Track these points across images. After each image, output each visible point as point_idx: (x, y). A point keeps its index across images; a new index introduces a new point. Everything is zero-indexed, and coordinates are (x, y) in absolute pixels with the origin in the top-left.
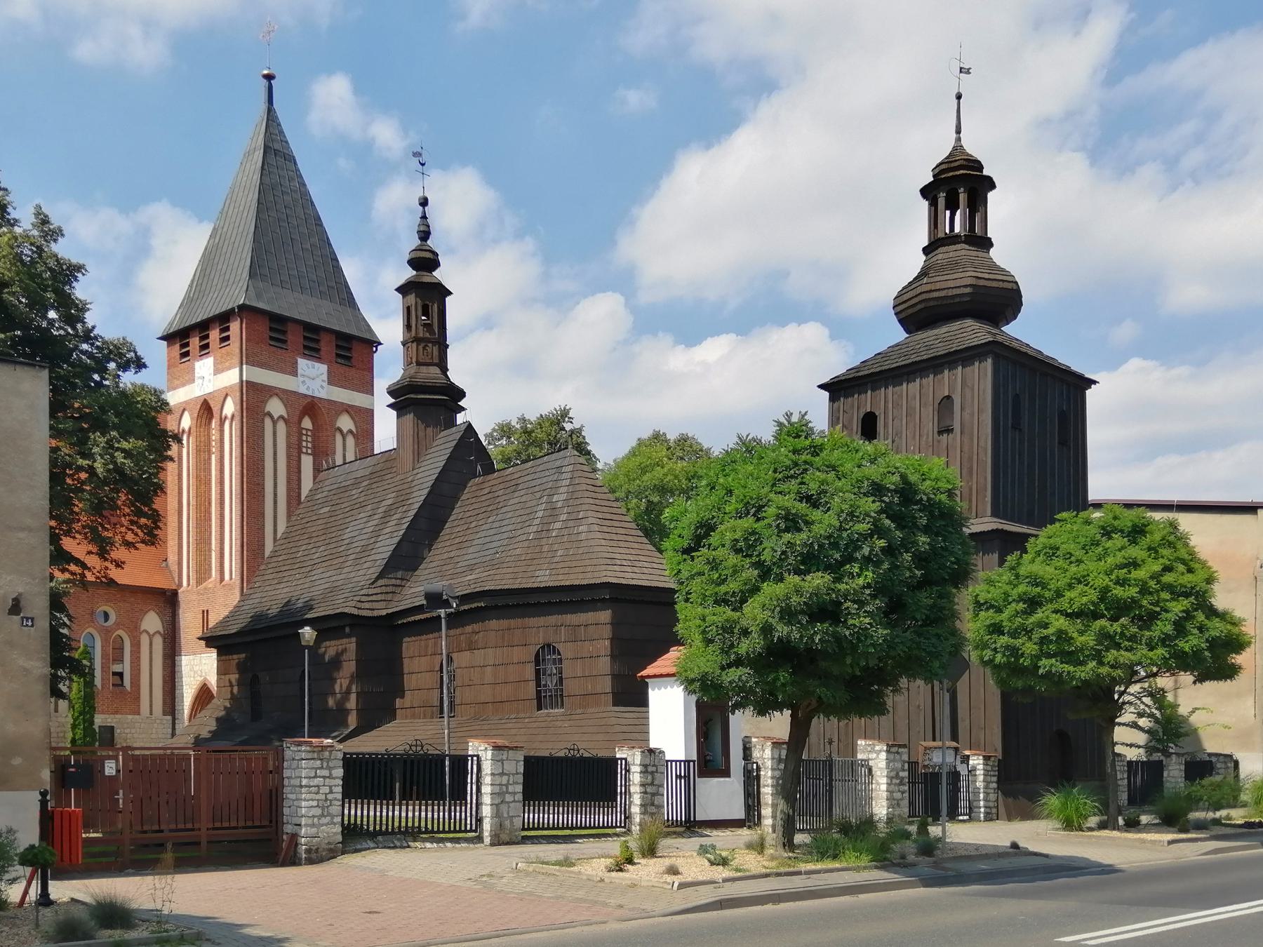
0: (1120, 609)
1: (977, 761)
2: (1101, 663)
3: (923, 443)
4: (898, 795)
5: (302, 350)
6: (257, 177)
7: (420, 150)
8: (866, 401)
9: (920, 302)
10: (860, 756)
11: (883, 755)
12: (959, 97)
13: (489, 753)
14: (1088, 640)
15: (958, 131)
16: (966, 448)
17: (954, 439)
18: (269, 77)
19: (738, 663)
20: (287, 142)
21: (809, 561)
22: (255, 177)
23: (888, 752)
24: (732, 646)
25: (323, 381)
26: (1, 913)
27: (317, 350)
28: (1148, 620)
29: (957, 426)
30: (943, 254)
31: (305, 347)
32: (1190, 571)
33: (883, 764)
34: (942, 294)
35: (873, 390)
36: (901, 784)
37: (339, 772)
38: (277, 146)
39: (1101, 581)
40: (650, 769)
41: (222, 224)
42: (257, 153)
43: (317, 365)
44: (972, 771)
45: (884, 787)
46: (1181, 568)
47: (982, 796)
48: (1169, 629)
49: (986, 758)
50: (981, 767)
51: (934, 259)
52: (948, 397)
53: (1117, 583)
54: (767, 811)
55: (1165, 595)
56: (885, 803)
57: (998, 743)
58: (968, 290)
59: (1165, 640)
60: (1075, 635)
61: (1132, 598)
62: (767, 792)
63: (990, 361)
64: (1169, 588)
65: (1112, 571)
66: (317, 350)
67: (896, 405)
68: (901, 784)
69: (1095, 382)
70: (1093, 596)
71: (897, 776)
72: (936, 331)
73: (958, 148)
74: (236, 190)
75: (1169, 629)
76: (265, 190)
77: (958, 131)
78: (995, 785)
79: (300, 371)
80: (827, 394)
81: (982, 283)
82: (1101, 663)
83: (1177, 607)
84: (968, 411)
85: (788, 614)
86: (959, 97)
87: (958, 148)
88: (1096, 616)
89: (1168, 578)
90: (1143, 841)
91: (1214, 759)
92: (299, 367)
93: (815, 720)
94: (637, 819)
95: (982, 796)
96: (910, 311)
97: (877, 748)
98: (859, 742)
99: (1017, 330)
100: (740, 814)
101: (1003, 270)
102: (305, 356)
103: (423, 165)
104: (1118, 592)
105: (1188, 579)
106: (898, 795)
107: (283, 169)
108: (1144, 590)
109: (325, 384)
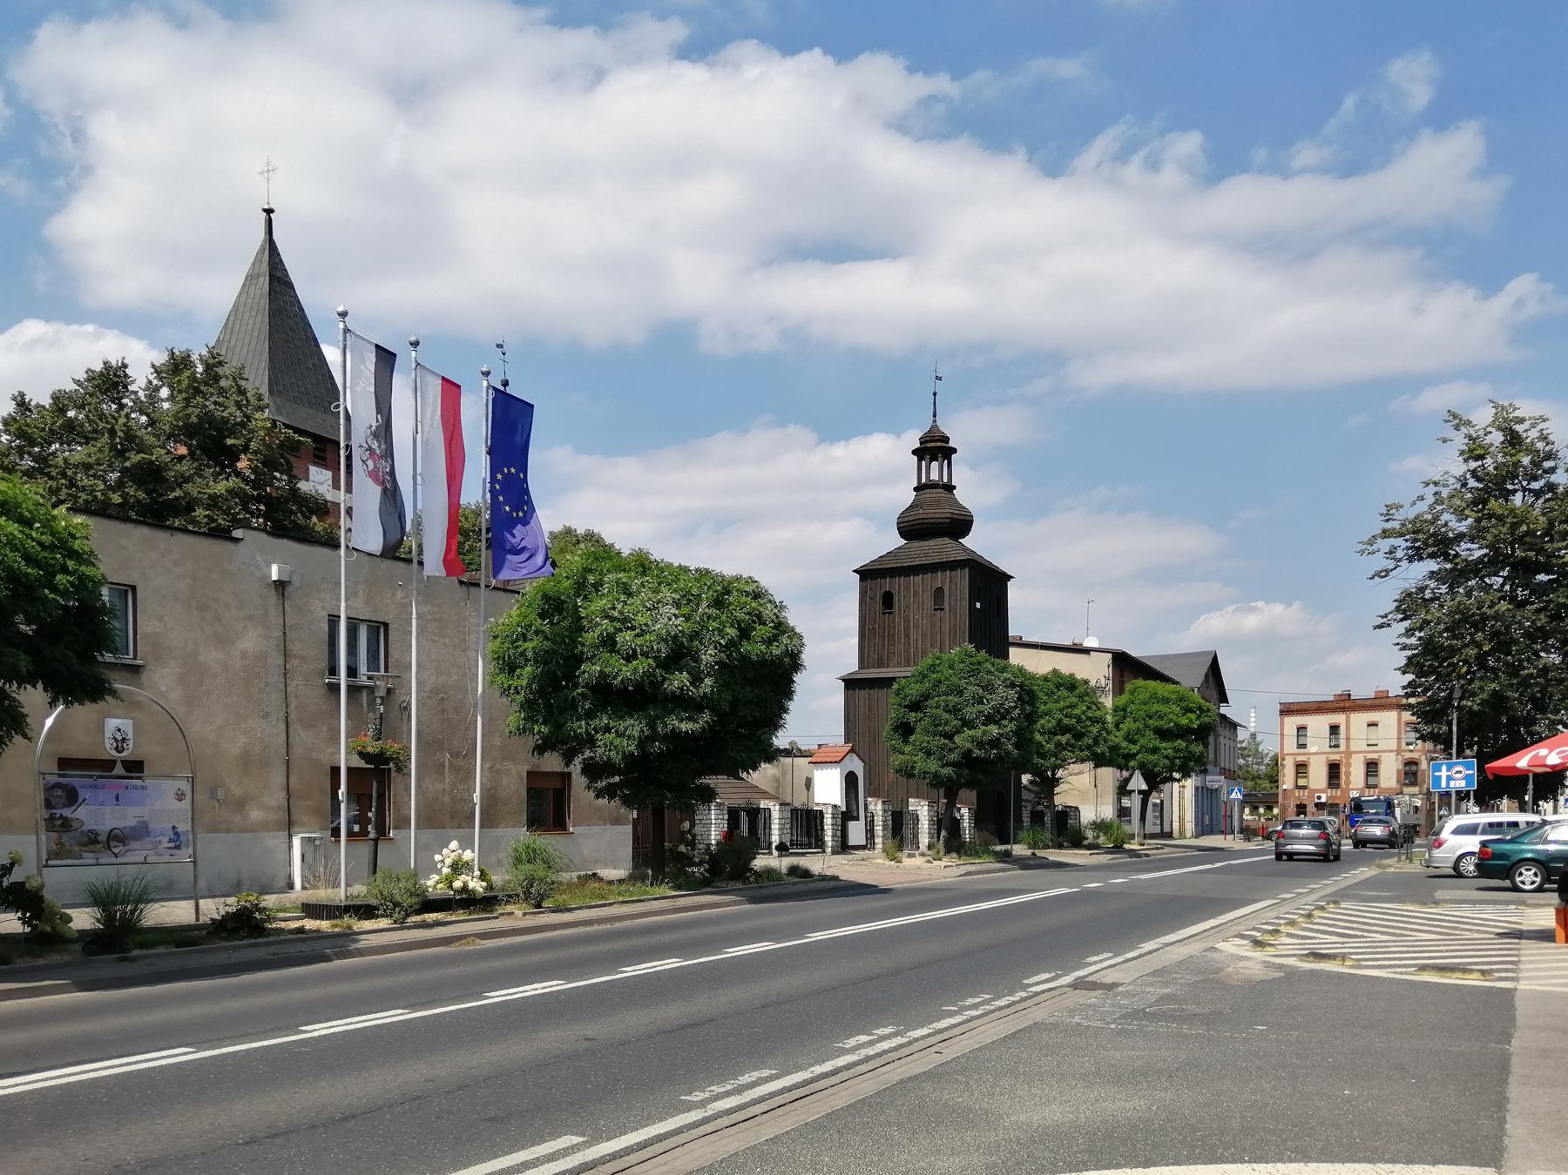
0: (1065, 730)
1: (965, 811)
2: (1057, 759)
3: (924, 615)
4: (932, 831)
5: (312, 458)
6: (265, 302)
7: (502, 343)
8: (887, 584)
9: (918, 524)
10: (910, 808)
11: (926, 808)
12: (935, 394)
13: (777, 808)
14: (1050, 746)
15: (935, 416)
16: (952, 621)
17: (945, 614)
18: (269, 211)
19: (948, 765)
20: (286, 270)
21: (989, 720)
22: (262, 301)
23: (928, 805)
24: (945, 756)
25: (329, 485)
26: (3, 967)
27: (324, 459)
28: (1079, 736)
29: (946, 606)
30: (929, 494)
31: (315, 456)
32: (1099, 709)
33: (926, 813)
34: (932, 521)
35: (890, 578)
36: (934, 824)
37: (726, 817)
38: (279, 274)
39: (1058, 716)
40: (835, 816)
41: (227, 338)
42: (261, 279)
43: (324, 471)
44: (962, 816)
45: (926, 826)
46: (1094, 707)
47: (967, 832)
48: (1091, 742)
49: (969, 809)
50: (967, 814)
51: (924, 496)
52: (941, 588)
53: (1066, 717)
54: (879, 840)
55: (1088, 723)
56: (927, 836)
57: (975, 801)
58: (947, 520)
59: (1089, 747)
60: (1044, 743)
61: (1073, 725)
62: (879, 829)
63: (967, 570)
64: (1089, 718)
65: (1063, 709)
66: (324, 459)
67: (907, 588)
68: (934, 824)
69: (1012, 577)
70: (1054, 722)
71: (932, 820)
72: (927, 543)
73: (934, 427)
74: (241, 309)
75: (1091, 742)
76: (273, 313)
77: (935, 416)
78: (973, 825)
79: (311, 477)
80: (858, 576)
81: (955, 516)
82: (1057, 759)
83: (1095, 729)
84: (953, 598)
85: (980, 745)
86: (935, 394)
87: (934, 427)
88: (1055, 734)
89: (1090, 714)
90: (1076, 854)
91: (1068, 810)
92: (311, 473)
93: (960, 792)
94: (830, 844)
95: (967, 832)
96: (910, 528)
97: (922, 804)
98: (910, 800)
99: (973, 542)
100: (1299, 784)
101: (964, 508)
102: (315, 464)
103: (504, 354)
104: (1066, 721)
105: (1098, 713)
106: (932, 831)
107: (285, 296)
108: (1079, 720)
109: (330, 488)
